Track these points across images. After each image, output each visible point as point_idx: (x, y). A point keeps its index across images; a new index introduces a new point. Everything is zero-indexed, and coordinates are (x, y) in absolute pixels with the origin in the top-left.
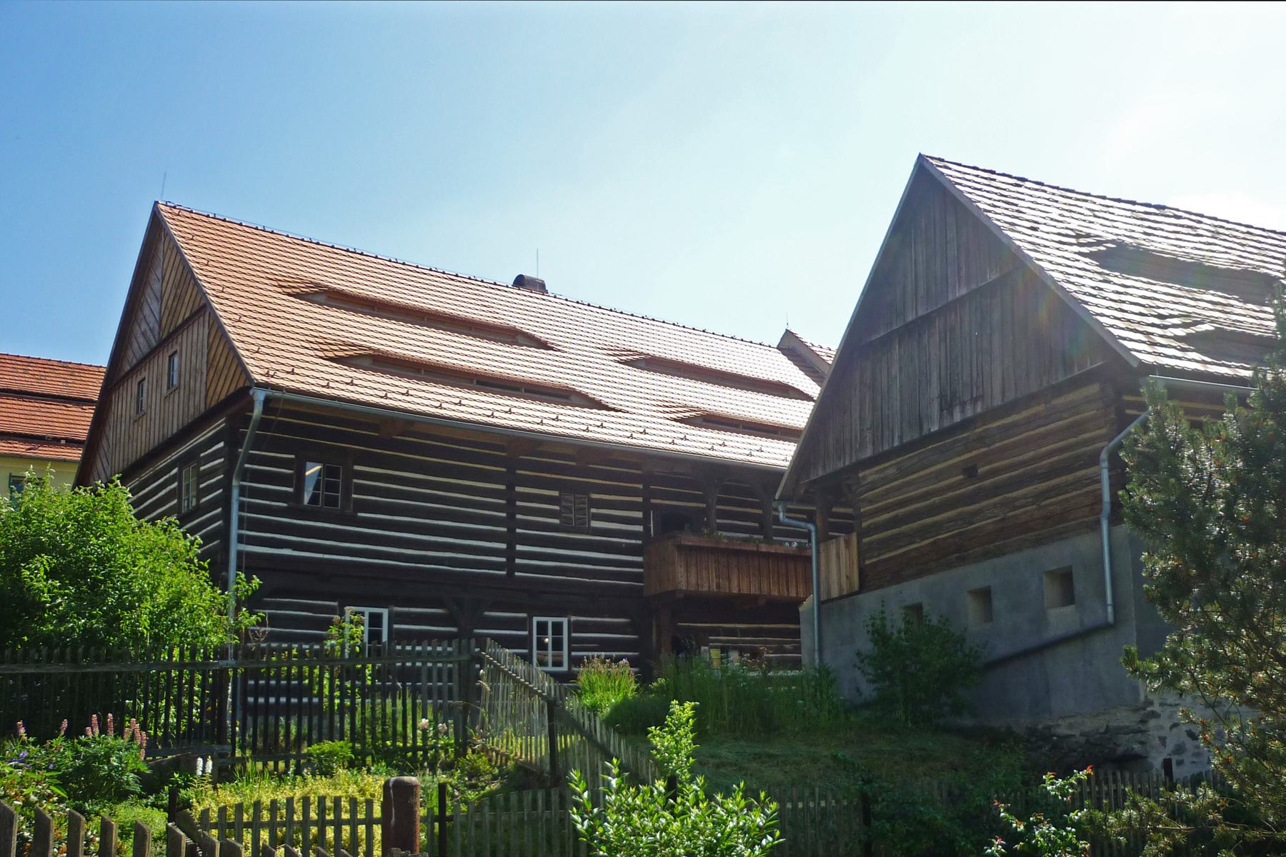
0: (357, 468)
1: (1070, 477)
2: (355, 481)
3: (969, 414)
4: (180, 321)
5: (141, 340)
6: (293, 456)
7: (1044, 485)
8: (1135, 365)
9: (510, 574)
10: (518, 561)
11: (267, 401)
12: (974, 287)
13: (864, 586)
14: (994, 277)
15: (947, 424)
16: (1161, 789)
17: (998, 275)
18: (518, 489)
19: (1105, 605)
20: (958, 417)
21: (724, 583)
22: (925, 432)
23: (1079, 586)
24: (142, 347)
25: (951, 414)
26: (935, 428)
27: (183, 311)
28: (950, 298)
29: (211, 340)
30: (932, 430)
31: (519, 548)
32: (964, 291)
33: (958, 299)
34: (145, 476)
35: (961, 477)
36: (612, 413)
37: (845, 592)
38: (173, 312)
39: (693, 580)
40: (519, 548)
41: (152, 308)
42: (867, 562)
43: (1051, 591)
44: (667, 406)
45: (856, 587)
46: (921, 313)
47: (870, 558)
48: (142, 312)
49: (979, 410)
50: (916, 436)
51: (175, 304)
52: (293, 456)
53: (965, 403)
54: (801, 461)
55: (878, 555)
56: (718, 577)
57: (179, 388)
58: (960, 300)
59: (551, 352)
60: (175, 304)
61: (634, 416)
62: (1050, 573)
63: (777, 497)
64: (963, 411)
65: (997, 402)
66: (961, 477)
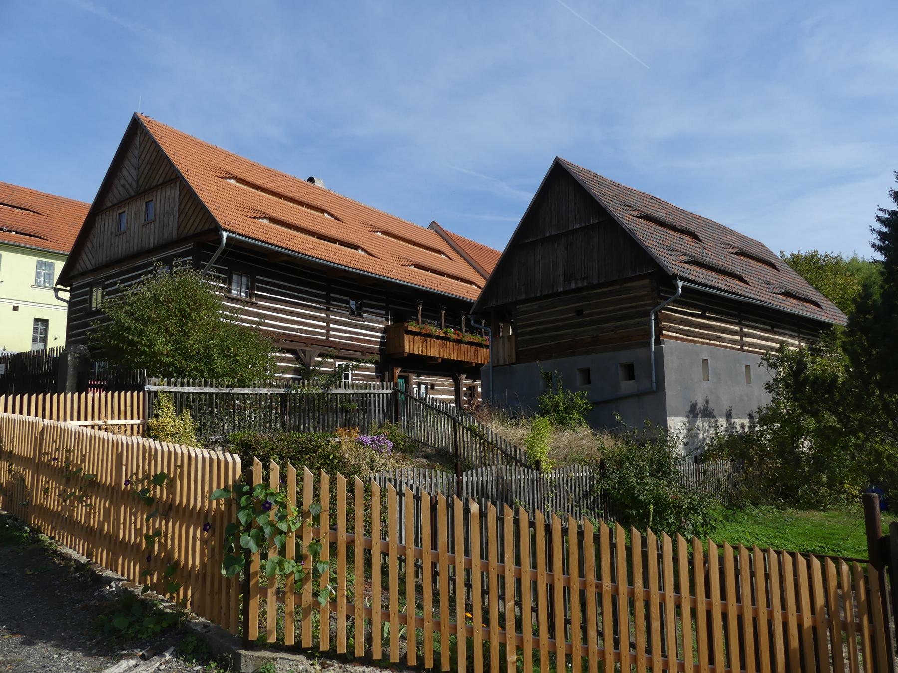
0: (257, 277)
1: (632, 321)
2: (257, 284)
3: (580, 285)
4: (154, 184)
5: (121, 189)
6: (227, 268)
7: (618, 323)
8: (670, 274)
9: (328, 338)
10: (331, 332)
11: (228, 238)
12: (584, 225)
13: (518, 361)
14: (594, 222)
15: (567, 288)
16: (807, 469)
17: (597, 221)
18: (332, 295)
19: (652, 382)
20: (573, 286)
21: (424, 350)
22: (555, 290)
23: (637, 372)
24: (121, 193)
25: (570, 284)
26: (560, 290)
27: (157, 177)
28: (570, 229)
29: (181, 197)
30: (559, 291)
31: (332, 325)
32: (578, 226)
33: (574, 229)
34: (124, 268)
35: (574, 314)
36: (373, 258)
37: (507, 363)
38: (137, 176)
39: (411, 348)
40: (332, 325)
41: (129, 174)
42: (520, 350)
43: (621, 373)
44: (398, 257)
45: (514, 361)
46: (553, 234)
47: (522, 348)
48: (121, 172)
49: (585, 284)
50: (550, 292)
51: (150, 173)
52: (227, 268)
53: (578, 279)
54: (484, 297)
55: (527, 346)
56: (422, 347)
57: (154, 221)
58: (577, 230)
59: (343, 224)
60: (150, 173)
61: (385, 262)
62: (621, 365)
63: (471, 312)
64: (576, 283)
65: (595, 282)
66: (574, 314)
